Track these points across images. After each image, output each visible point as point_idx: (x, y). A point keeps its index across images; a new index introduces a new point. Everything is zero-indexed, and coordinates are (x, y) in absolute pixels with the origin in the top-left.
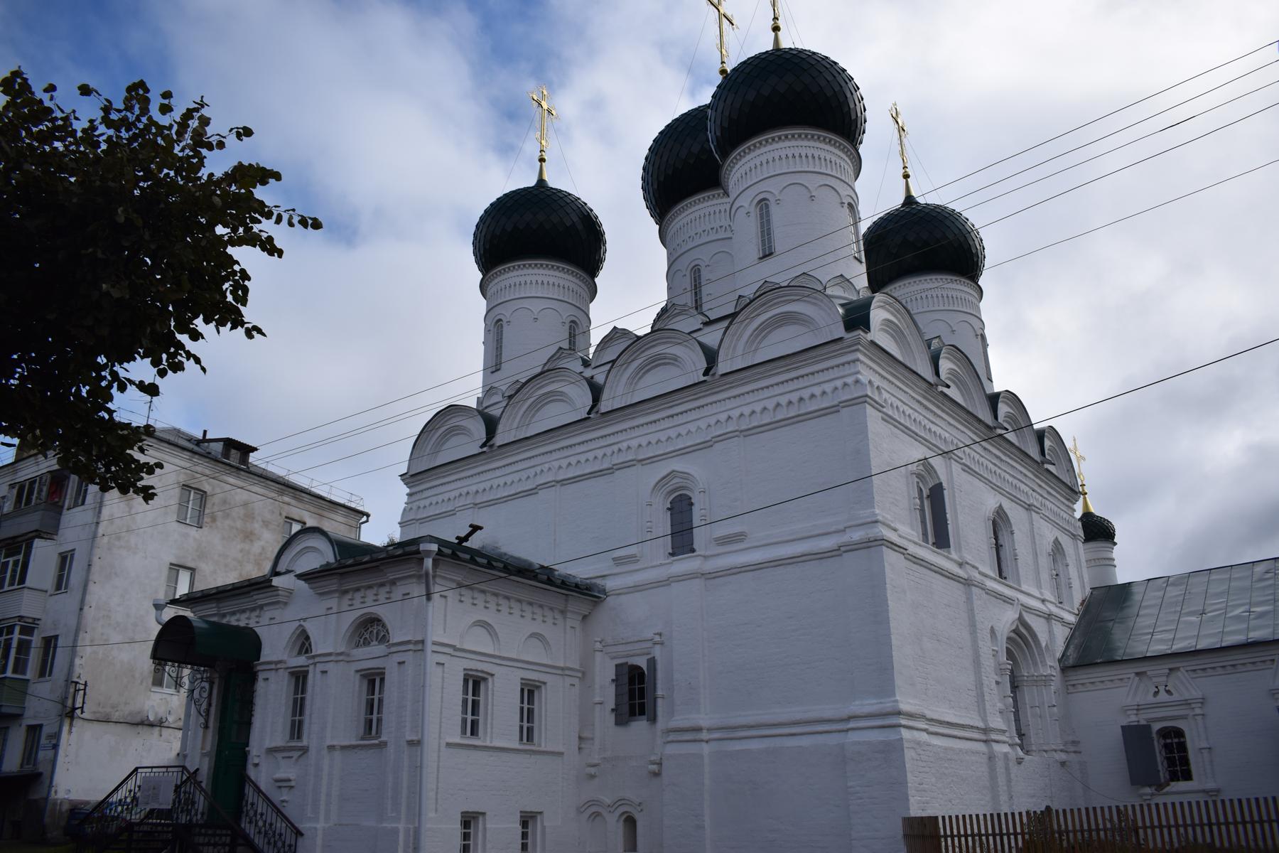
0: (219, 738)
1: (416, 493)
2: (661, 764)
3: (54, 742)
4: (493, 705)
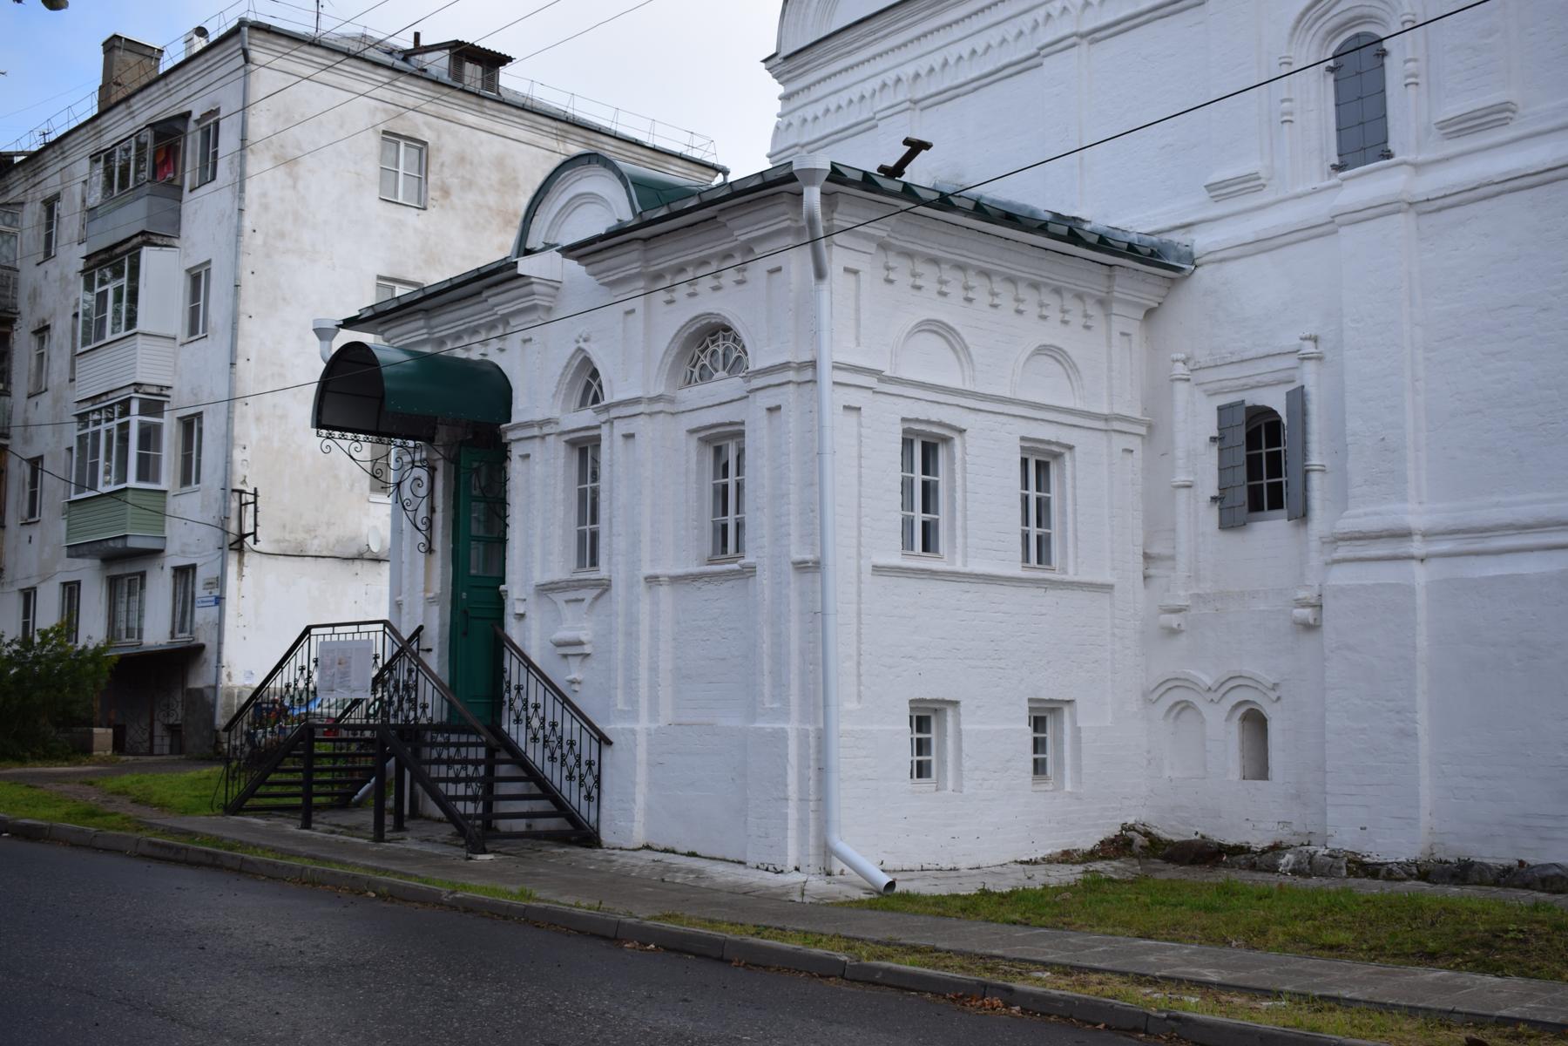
1: (797, 93)
2: (1321, 606)
3: (216, 592)
4: (965, 491)
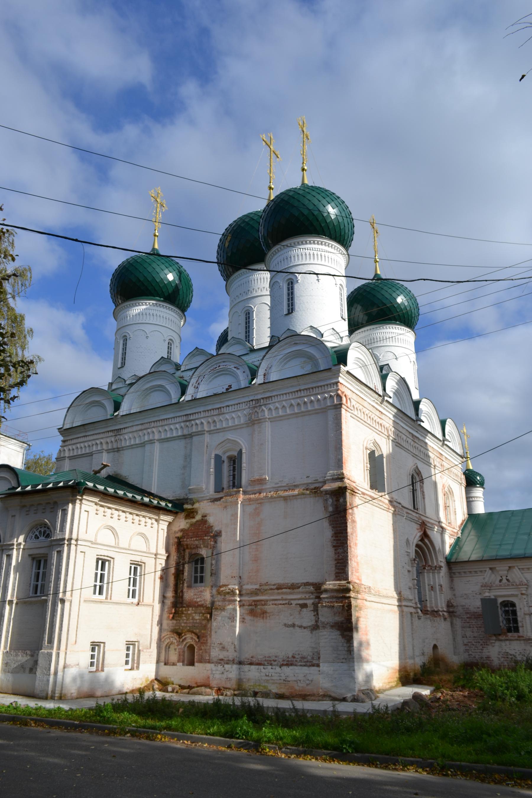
0: (351, 619)
1: (67, 440)
